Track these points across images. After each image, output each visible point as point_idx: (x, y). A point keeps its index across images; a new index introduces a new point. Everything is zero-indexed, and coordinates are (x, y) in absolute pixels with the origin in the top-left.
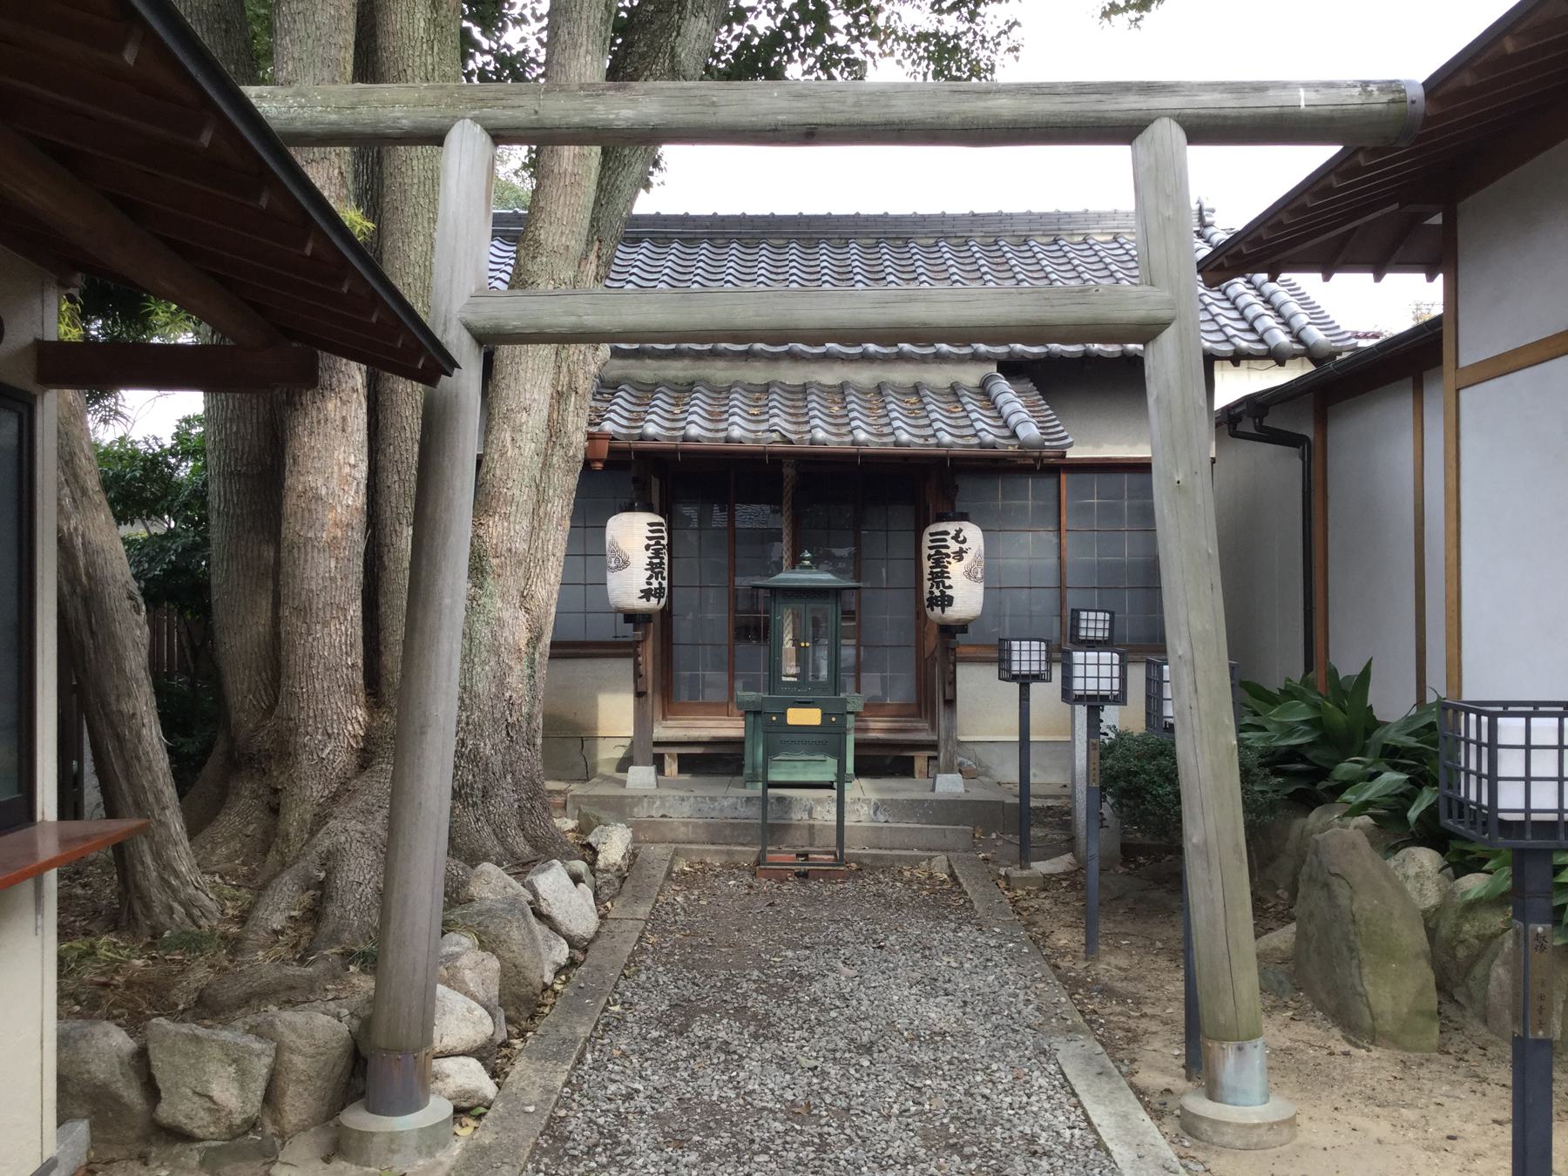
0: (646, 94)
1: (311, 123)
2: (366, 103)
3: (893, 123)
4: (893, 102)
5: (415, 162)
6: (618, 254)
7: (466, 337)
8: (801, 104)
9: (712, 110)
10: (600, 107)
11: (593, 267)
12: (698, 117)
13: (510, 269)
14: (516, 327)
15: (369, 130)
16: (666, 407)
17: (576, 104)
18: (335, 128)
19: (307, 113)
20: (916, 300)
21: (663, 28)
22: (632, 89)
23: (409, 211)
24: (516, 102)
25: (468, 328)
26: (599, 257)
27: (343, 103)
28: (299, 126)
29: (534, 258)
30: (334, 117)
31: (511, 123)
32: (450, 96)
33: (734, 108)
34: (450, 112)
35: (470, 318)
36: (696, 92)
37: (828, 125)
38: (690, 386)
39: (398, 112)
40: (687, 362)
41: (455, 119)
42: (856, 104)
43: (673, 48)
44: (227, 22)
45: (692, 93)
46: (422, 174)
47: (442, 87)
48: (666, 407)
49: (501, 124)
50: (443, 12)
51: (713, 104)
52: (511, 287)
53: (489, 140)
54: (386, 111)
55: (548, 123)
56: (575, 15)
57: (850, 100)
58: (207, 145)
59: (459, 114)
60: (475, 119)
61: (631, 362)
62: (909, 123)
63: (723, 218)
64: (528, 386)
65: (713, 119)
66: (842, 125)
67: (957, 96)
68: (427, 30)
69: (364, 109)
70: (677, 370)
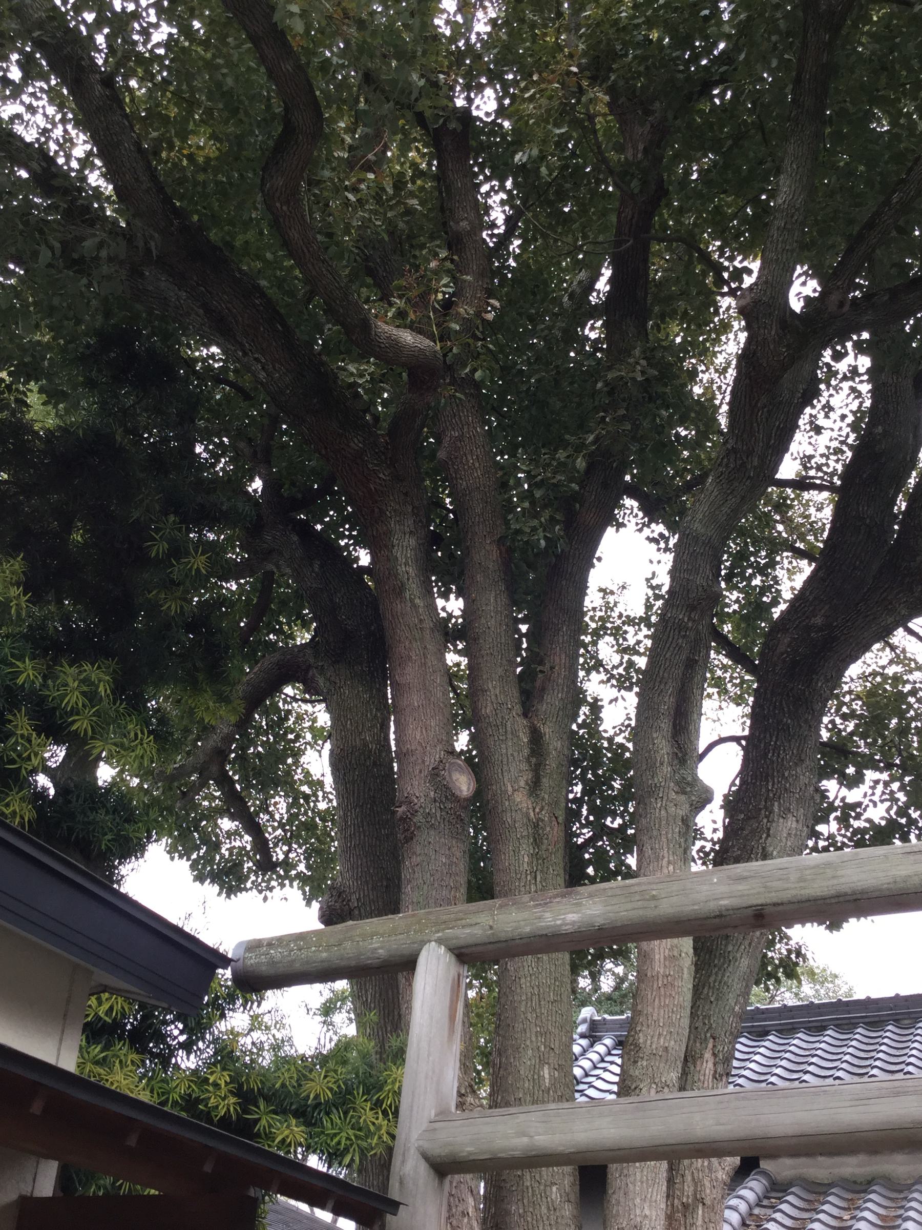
0: (591, 896)
1: (307, 963)
2: (351, 939)
3: (846, 894)
4: (839, 873)
5: (523, 980)
6: (738, 1046)
7: (423, 1167)
8: (741, 887)
9: (652, 904)
10: (548, 915)
11: (710, 1065)
12: (641, 912)
13: (735, 1063)
14: (470, 1153)
15: (353, 963)
16: (835, 1211)
17: (525, 915)
18: (326, 965)
19: (304, 954)
20: (906, 1093)
21: (753, 832)
22: (578, 893)
23: (519, 1026)
24: (474, 920)
25: (426, 1157)
26: (714, 1055)
27: (332, 941)
28: (297, 966)
29: (635, 1062)
30: (324, 955)
31: (471, 941)
32: (419, 922)
33: (675, 899)
34: (419, 937)
35: (426, 1145)
36: (637, 888)
37: (775, 904)
38: (870, 1182)
39: (376, 943)
40: (862, 1158)
41: (423, 943)
42: (801, 879)
43: (764, 848)
44: (388, 879)
45: (633, 889)
46: (530, 990)
47: (413, 916)
48: (835, 1211)
49: (462, 942)
50: (544, 847)
51: (654, 898)
52: (618, 1094)
53: (453, 959)
54: (366, 943)
55: (503, 936)
56: (655, 833)
57: (793, 877)
58: (345, 981)
59: (425, 938)
60: (440, 942)
61: (802, 1160)
62: (863, 892)
63: (908, 999)
64: (638, 1201)
65: (656, 913)
66: (790, 903)
67: (912, 857)
68: (530, 864)
69: (348, 945)
70: (851, 1166)
